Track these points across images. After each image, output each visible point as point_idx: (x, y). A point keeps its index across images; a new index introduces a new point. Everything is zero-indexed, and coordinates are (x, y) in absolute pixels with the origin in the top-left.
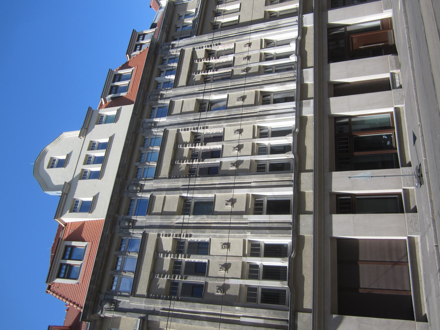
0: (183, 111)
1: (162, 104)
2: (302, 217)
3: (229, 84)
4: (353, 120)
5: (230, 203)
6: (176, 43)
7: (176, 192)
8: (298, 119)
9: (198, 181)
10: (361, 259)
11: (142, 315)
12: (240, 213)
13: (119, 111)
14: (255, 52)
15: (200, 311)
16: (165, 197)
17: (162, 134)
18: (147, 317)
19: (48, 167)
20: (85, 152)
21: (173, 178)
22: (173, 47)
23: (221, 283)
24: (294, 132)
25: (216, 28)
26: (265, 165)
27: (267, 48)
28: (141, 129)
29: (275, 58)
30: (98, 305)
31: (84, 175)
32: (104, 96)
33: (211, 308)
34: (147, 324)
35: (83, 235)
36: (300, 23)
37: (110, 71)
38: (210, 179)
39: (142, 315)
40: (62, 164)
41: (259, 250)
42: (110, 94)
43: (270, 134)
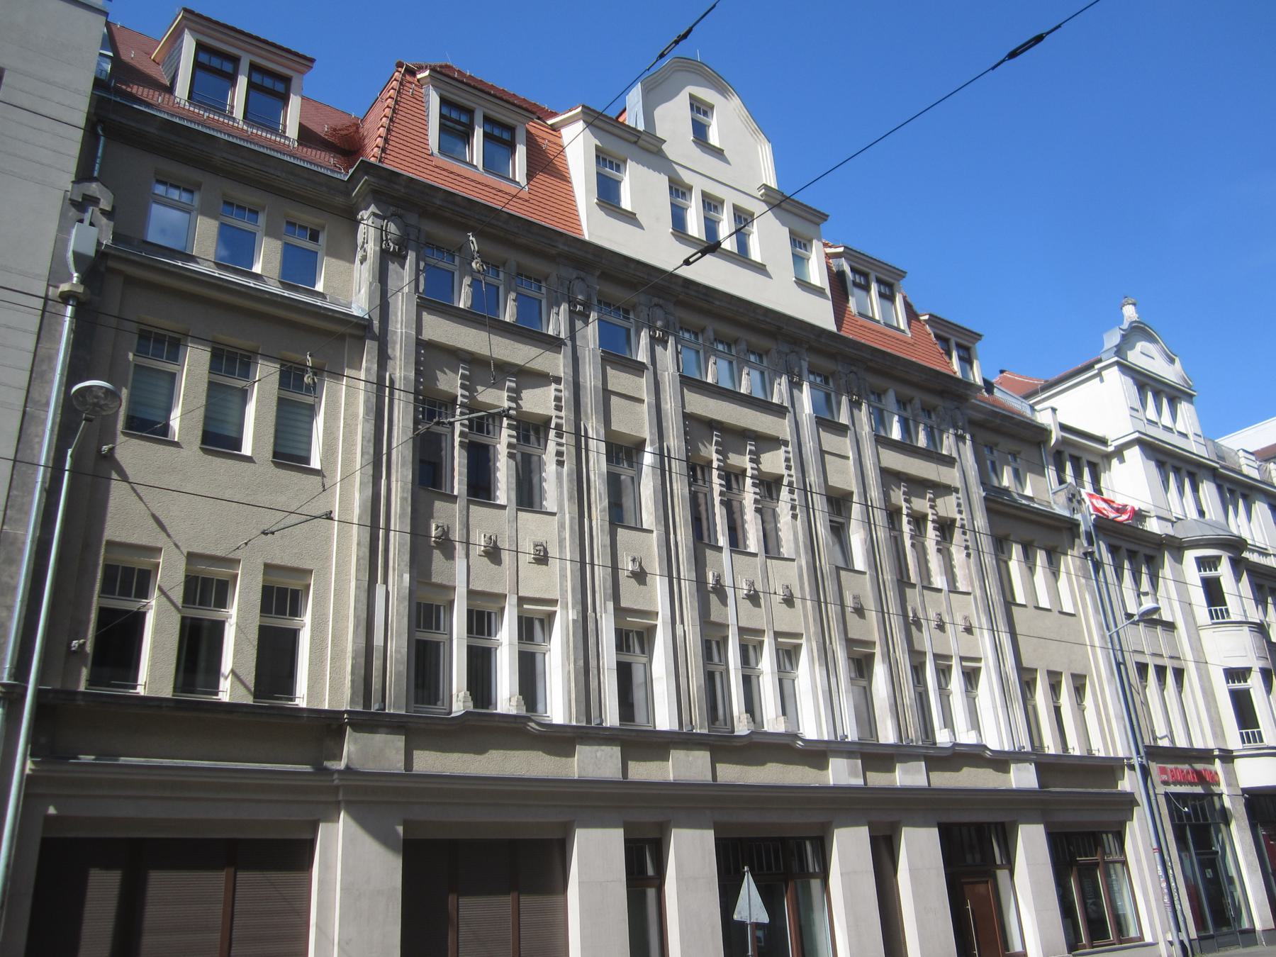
0: (613, 398)
1: (839, 404)
2: (397, 743)
3: (888, 576)
4: (816, 884)
5: (637, 568)
6: (968, 450)
7: (655, 430)
8: (821, 747)
9: (680, 488)
10: (524, 899)
11: (376, 323)
12: (616, 597)
13: (818, 291)
14: (954, 644)
15: (393, 479)
16: (641, 401)
17: (550, 333)
18: (374, 338)
19: (692, 97)
20: (730, 199)
21: (418, 353)
22: (960, 438)
23: (457, 535)
24: (530, 719)
25: (1001, 545)
26: (438, 628)
27: (777, 651)
28: (785, 348)
29: (748, 672)
30: (392, 209)
31: (679, 190)
32: (849, 253)
33: (402, 507)
34: (352, 336)
35: (541, 177)
36: (1017, 757)
37: (901, 274)
38: (686, 521)
39: (376, 323)
40: (700, 132)
41: (281, 611)
42: (853, 270)
43: (529, 648)
